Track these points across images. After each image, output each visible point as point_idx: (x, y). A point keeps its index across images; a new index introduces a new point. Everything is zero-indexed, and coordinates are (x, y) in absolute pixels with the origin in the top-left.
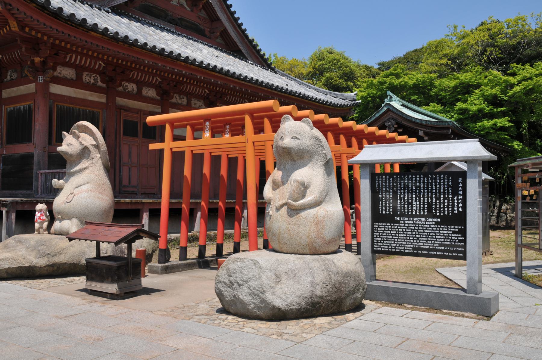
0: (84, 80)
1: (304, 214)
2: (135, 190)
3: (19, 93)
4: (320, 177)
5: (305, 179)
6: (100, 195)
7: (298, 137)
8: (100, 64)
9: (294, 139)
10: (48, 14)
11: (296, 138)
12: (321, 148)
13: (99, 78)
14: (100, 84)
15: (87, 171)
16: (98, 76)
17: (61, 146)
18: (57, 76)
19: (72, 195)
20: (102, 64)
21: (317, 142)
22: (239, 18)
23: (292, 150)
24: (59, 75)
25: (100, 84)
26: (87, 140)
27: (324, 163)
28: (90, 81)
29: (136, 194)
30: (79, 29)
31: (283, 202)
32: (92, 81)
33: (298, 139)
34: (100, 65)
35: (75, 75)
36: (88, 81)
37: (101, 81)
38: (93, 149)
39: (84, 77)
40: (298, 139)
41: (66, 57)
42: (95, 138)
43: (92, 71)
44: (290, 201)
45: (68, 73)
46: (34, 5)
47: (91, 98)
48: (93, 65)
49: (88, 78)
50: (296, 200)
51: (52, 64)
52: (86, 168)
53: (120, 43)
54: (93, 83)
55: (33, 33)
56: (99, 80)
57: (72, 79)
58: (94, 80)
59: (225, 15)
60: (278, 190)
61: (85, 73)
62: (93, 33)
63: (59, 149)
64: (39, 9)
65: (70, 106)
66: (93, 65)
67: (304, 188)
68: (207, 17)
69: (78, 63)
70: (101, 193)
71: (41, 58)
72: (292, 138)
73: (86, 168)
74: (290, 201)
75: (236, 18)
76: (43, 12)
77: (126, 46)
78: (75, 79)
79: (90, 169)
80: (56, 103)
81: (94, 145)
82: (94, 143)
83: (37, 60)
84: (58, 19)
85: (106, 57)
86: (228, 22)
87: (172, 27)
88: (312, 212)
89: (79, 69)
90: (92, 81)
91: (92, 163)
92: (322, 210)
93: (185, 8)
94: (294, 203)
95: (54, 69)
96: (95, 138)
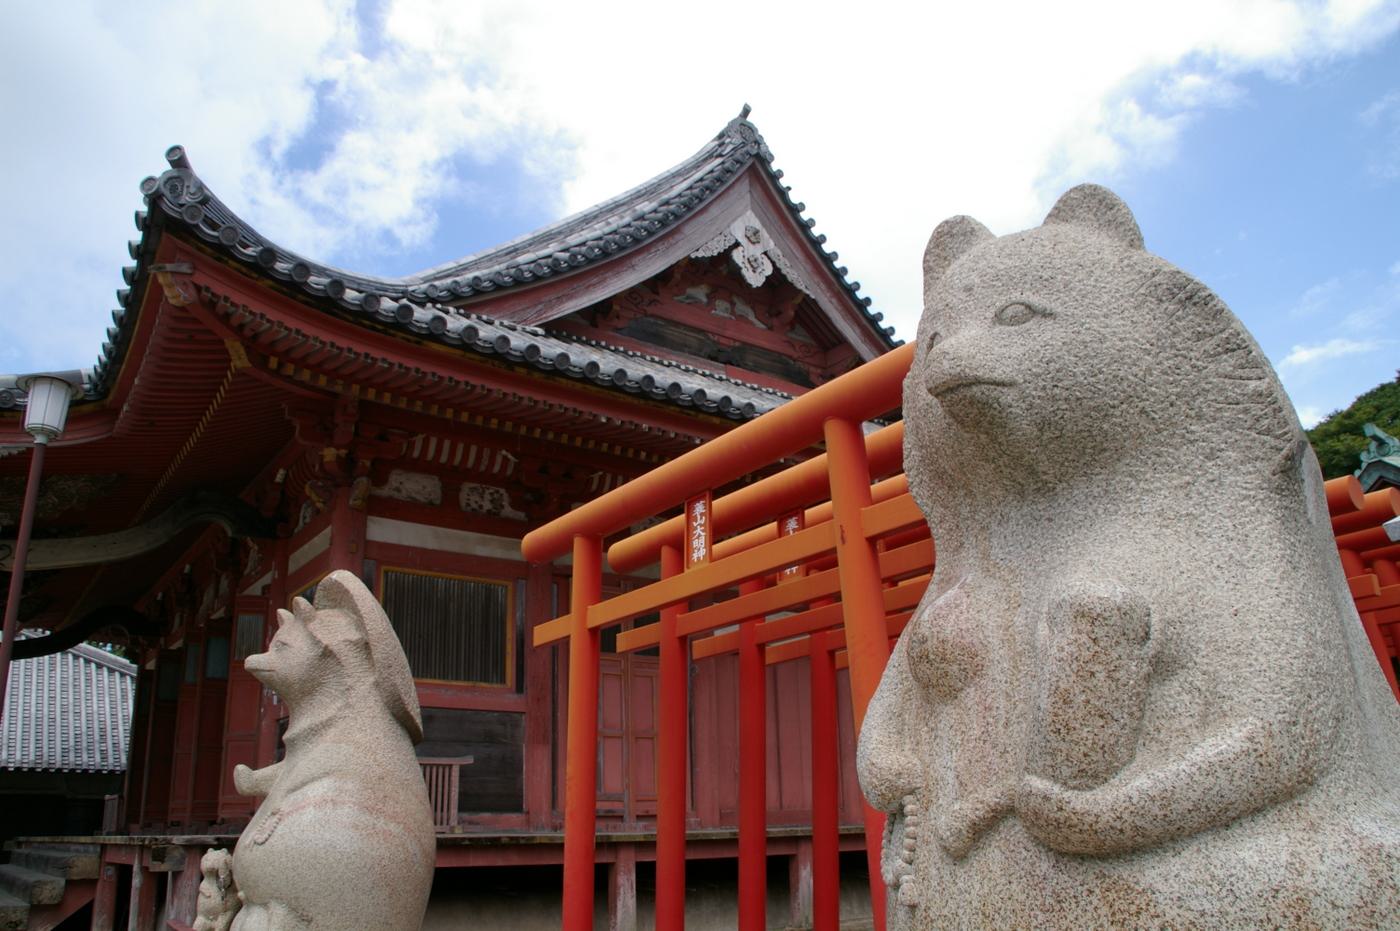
0: (463, 504)
1: (1169, 879)
2: (617, 806)
3: (311, 556)
4: (1265, 572)
5: (1143, 591)
6: (366, 818)
7: (1036, 300)
8: (505, 458)
9: (1015, 320)
10: (306, 303)
11: (1032, 311)
12: (1227, 364)
13: (506, 496)
14: (508, 511)
15: (332, 733)
16: (502, 491)
17: (264, 649)
18: (391, 498)
19: (275, 819)
20: (510, 456)
21: (1190, 319)
22: (892, 330)
23: (1008, 396)
24: (396, 495)
25: (508, 511)
26: (334, 628)
27: (1266, 468)
28: (481, 507)
29: (622, 817)
30: (394, 336)
31: (992, 795)
32: (487, 506)
33: (1047, 314)
34: (505, 458)
35: (439, 491)
36: (474, 506)
37: (513, 505)
38: (351, 659)
39: (463, 497)
40: (1047, 314)
41: (411, 446)
42: (360, 624)
43: (486, 479)
44: (1038, 784)
45: (419, 487)
46: (270, 282)
47: (482, 551)
48: (485, 462)
49: (475, 498)
50: (1090, 776)
51: (368, 463)
52: (327, 724)
53: (517, 369)
54: (489, 511)
55: (323, 381)
56: (505, 503)
57: (431, 503)
58: (492, 501)
59: (856, 328)
60: (949, 714)
61: (466, 487)
62: (436, 347)
63: (253, 661)
64: (283, 292)
65: (424, 573)
66: (485, 462)
67: (1136, 661)
68: (813, 343)
69: (444, 459)
70: (370, 810)
71: (338, 448)
72: (999, 318)
73: (327, 724)
74: (1038, 784)
75: (885, 330)
76: (294, 298)
77: (536, 375)
78: (438, 502)
79: (342, 725)
80: (384, 568)
81: (355, 643)
82: (355, 635)
83: (329, 454)
84: (336, 315)
85: (495, 421)
86: (864, 342)
87: (716, 368)
88: (1258, 854)
89: (451, 477)
90: (487, 506)
91: (348, 706)
92: (1331, 839)
93: (752, 323)
94: (1081, 801)
95: (380, 479)
96: (360, 624)
